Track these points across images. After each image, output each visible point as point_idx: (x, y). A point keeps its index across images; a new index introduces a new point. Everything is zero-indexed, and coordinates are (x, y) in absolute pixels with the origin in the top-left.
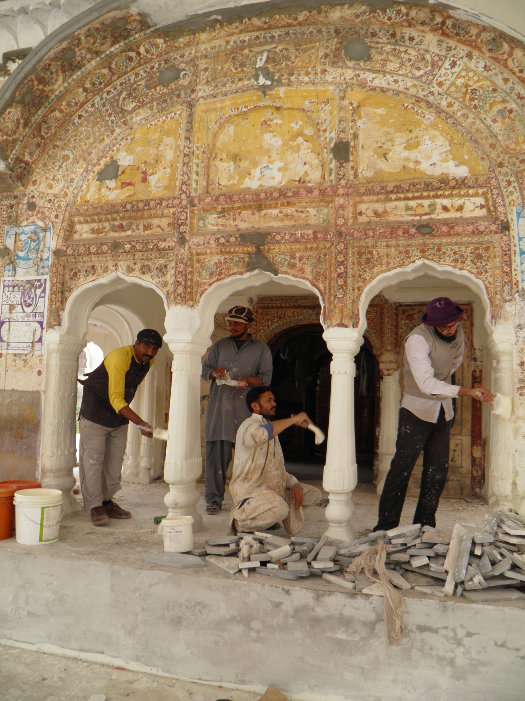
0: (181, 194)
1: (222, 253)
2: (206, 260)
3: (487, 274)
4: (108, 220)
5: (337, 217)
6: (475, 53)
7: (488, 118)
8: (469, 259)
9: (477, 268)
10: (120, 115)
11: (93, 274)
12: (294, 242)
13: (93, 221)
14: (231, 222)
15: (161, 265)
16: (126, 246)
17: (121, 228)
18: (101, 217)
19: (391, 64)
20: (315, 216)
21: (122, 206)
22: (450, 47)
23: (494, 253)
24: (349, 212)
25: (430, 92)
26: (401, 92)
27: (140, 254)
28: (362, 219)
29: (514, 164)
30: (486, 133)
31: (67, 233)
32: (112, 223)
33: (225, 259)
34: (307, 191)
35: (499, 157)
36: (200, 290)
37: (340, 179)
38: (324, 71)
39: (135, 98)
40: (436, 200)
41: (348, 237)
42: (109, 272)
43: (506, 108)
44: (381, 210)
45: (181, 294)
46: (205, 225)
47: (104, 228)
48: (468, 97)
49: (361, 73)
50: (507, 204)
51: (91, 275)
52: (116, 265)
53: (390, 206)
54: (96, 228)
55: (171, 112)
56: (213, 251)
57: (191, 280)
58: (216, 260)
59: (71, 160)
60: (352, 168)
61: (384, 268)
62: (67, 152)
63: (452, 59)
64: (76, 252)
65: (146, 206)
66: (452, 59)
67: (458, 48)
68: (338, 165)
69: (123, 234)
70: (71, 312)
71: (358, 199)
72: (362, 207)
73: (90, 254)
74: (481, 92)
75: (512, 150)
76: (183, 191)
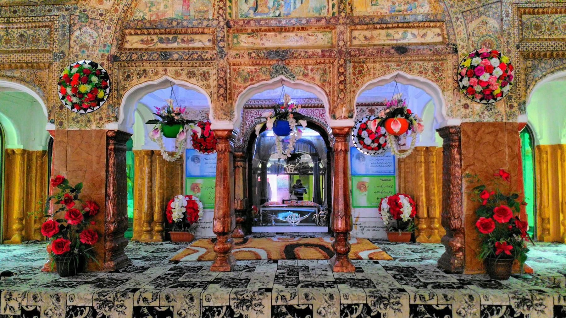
1: (253, 64)
5: (339, 40)
8: (430, 71)
9: (436, 77)
11: (145, 77)
13: (143, 34)
15: (204, 72)
16: (174, 55)
18: (150, 30)
24: (347, 36)
27: (187, 62)
28: (355, 42)
31: (120, 42)
32: (159, 36)
33: (256, 69)
36: (237, 91)
37: (341, 12)
41: (346, 55)
42: (160, 75)
45: (223, 94)
46: (238, 43)
47: (152, 40)
50: (456, 34)
51: (143, 77)
52: (165, 70)
53: (376, 32)
56: (246, 62)
57: (230, 84)
58: (249, 70)
60: (349, 4)
61: (371, 77)
64: (129, 58)
70: (25, 94)
71: (353, 28)
72: (355, 33)
73: (142, 60)
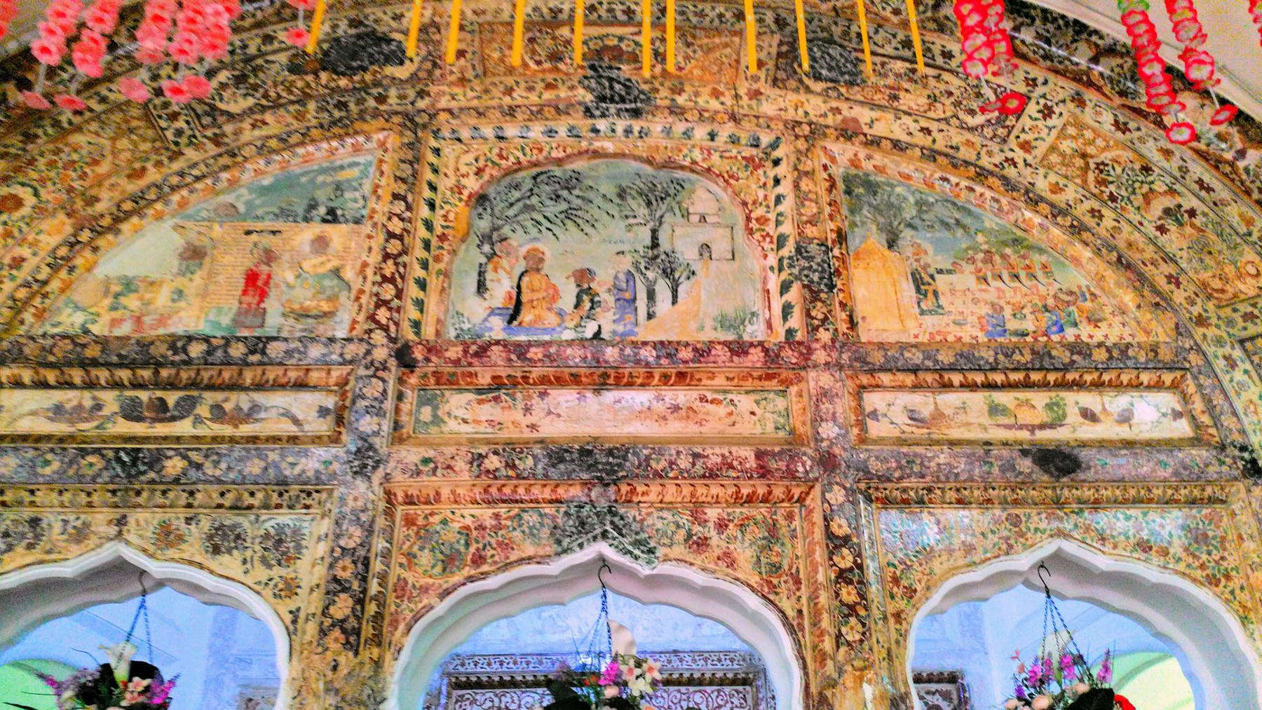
0: (370, 331)
2: (436, 519)
3: (1231, 584)
4: (117, 385)
6: (1090, 96)
7: (1145, 223)
10: (206, 120)
11: (30, 547)
12: (704, 477)
14: (518, 415)
16: (168, 463)
17: (161, 411)
19: (908, 95)
20: (753, 413)
21: (173, 347)
22: (1034, 80)
23: (1237, 528)
25: (1007, 160)
26: (940, 153)
27: (214, 490)
29: (1230, 322)
30: (1150, 252)
32: (129, 393)
34: (731, 350)
35: (1193, 303)
37: (816, 329)
38: (755, 95)
39: (255, 88)
40: (1063, 394)
42: (93, 540)
43: (1180, 206)
44: (926, 412)
45: (343, 621)
46: (437, 420)
47: (98, 407)
48: (1091, 177)
49: (844, 106)
50: (1240, 411)
51: (20, 549)
52: (121, 522)
53: (950, 400)
54: (68, 406)
55: (356, 133)
57: (383, 577)
58: (468, 521)
59: (25, 211)
62: (17, 190)
63: (1042, 101)
65: (253, 352)
66: (1042, 101)
67: (1050, 84)
68: (808, 295)
69: (161, 429)
71: (865, 380)
74: (1119, 170)
75: (1216, 291)
76: (377, 322)
